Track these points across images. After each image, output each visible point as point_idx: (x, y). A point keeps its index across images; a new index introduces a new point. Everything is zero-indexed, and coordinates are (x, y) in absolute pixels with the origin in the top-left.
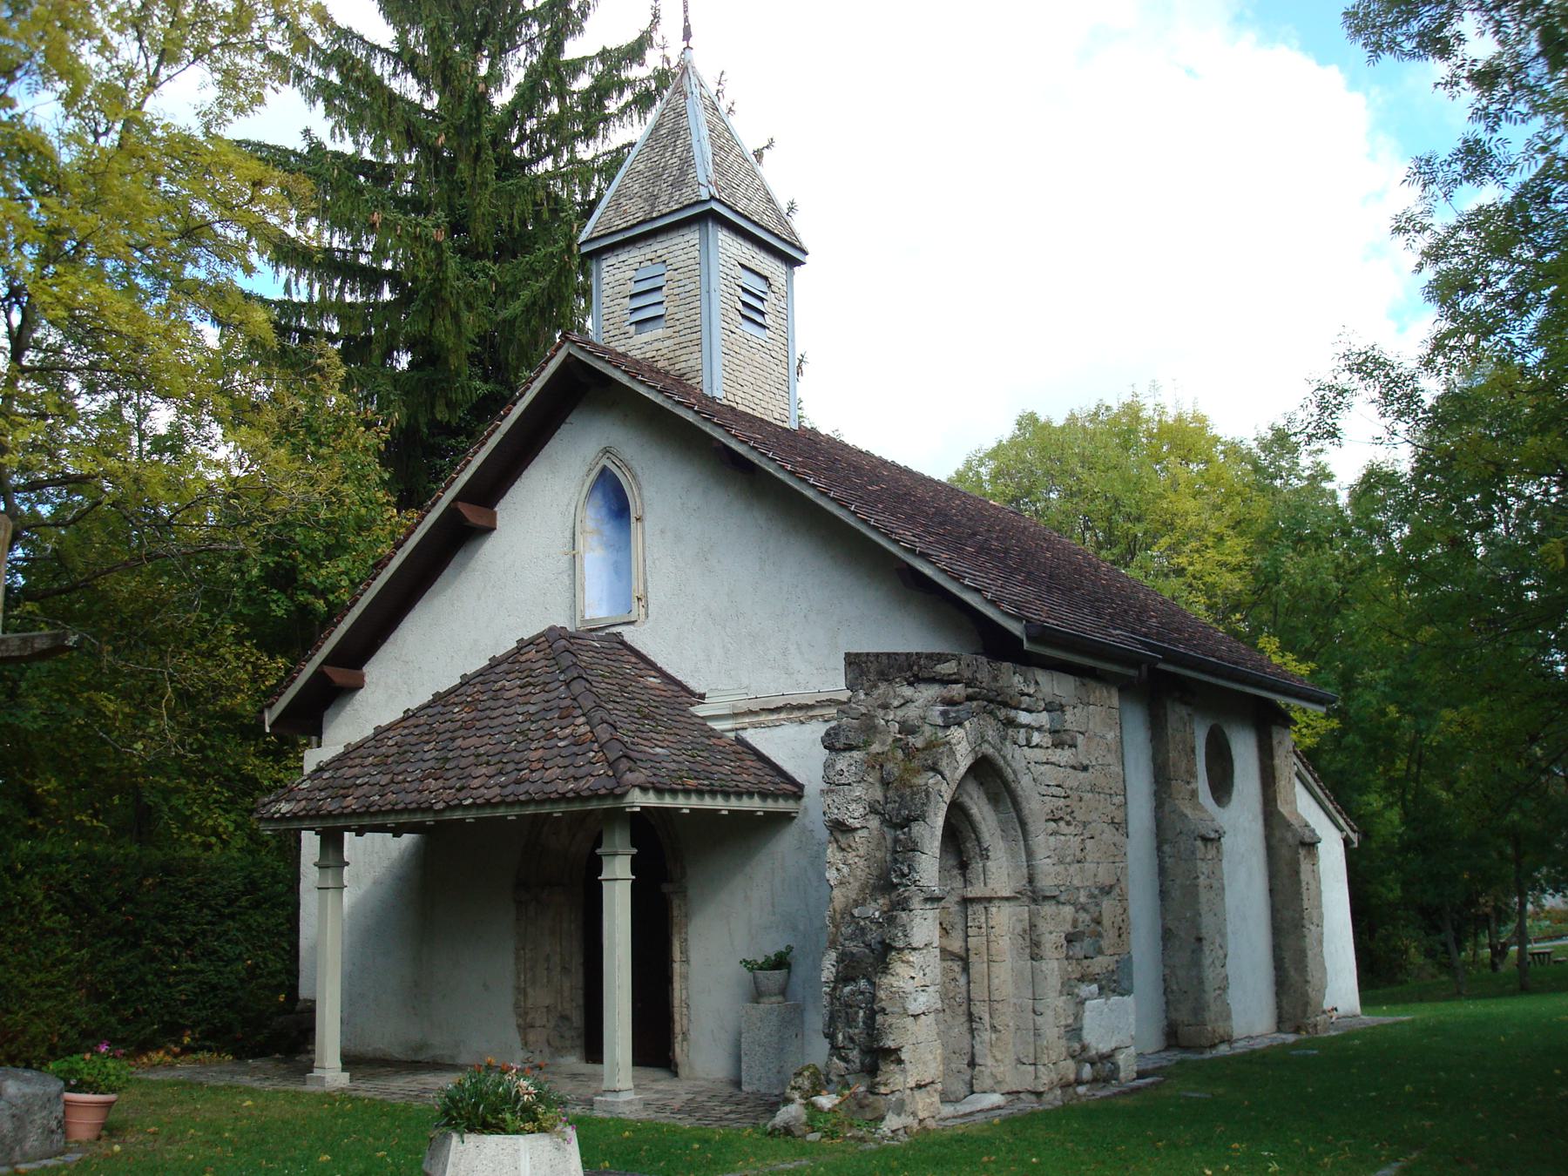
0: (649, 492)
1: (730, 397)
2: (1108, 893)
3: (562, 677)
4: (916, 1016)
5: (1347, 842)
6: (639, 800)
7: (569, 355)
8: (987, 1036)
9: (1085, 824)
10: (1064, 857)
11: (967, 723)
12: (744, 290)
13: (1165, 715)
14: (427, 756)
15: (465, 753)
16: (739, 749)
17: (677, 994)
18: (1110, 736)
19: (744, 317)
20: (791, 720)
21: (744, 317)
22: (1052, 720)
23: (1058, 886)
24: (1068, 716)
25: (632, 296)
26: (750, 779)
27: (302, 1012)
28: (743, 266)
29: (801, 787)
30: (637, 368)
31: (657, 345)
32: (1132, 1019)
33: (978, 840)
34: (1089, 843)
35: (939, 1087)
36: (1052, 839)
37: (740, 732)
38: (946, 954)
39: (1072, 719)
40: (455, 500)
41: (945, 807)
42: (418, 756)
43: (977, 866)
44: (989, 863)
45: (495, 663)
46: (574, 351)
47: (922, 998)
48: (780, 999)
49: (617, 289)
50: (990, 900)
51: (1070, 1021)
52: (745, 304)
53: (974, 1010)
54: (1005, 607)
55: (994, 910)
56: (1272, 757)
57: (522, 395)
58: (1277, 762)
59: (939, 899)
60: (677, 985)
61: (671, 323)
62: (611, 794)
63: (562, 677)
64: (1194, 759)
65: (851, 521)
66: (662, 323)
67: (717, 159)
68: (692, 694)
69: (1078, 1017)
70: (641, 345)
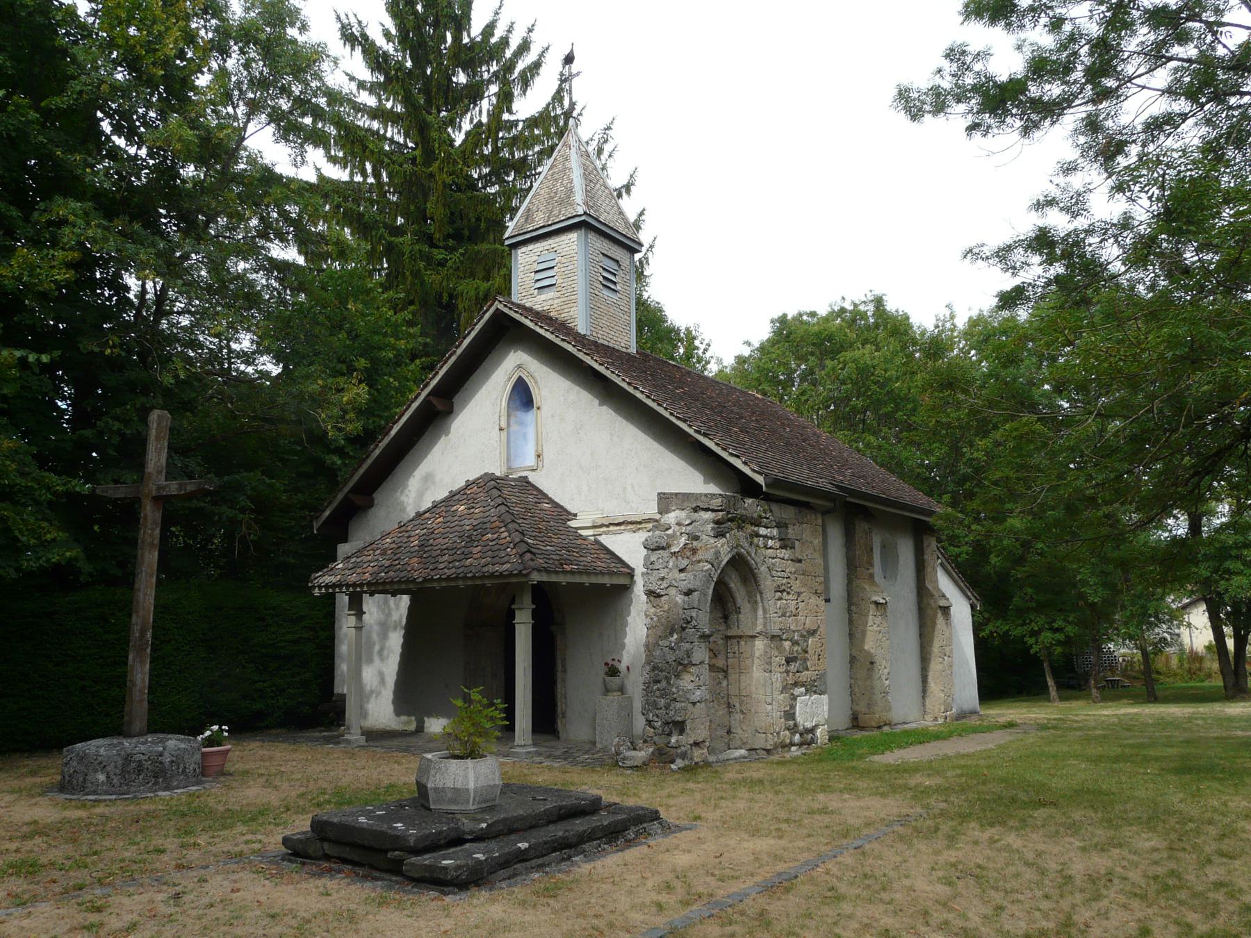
0: (544, 392)
1: (595, 334)
2: (812, 634)
3: (492, 503)
4: (694, 704)
5: (973, 607)
6: (536, 577)
7: (497, 309)
8: (738, 716)
9: (799, 594)
10: (785, 613)
11: (728, 535)
12: (604, 269)
13: (854, 529)
14: (413, 550)
15: (435, 548)
16: (597, 547)
17: (559, 690)
18: (816, 542)
19: (604, 285)
20: (629, 531)
21: (604, 285)
22: (780, 533)
23: (781, 629)
24: (790, 531)
25: (536, 272)
26: (602, 565)
27: (336, 701)
28: (603, 254)
29: (633, 570)
30: (540, 317)
31: (550, 302)
32: (826, 708)
33: (734, 602)
34: (801, 605)
35: (707, 744)
36: (779, 602)
37: (598, 537)
38: (712, 668)
39: (792, 532)
40: (429, 394)
41: (713, 584)
42: (408, 549)
43: (734, 617)
44: (741, 616)
45: (453, 495)
46: (501, 307)
47: (698, 693)
48: (619, 693)
49: (526, 268)
50: (740, 637)
51: (787, 709)
52: (604, 277)
53: (731, 701)
54: (753, 466)
55: (743, 643)
56: (923, 554)
57: (469, 333)
58: (926, 557)
59: (709, 636)
60: (559, 686)
61: (559, 289)
62: (520, 574)
63: (492, 503)
64: (872, 556)
65: (666, 414)
66: (553, 288)
67: (589, 188)
68: (569, 513)
69: (793, 707)
70: (540, 302)
